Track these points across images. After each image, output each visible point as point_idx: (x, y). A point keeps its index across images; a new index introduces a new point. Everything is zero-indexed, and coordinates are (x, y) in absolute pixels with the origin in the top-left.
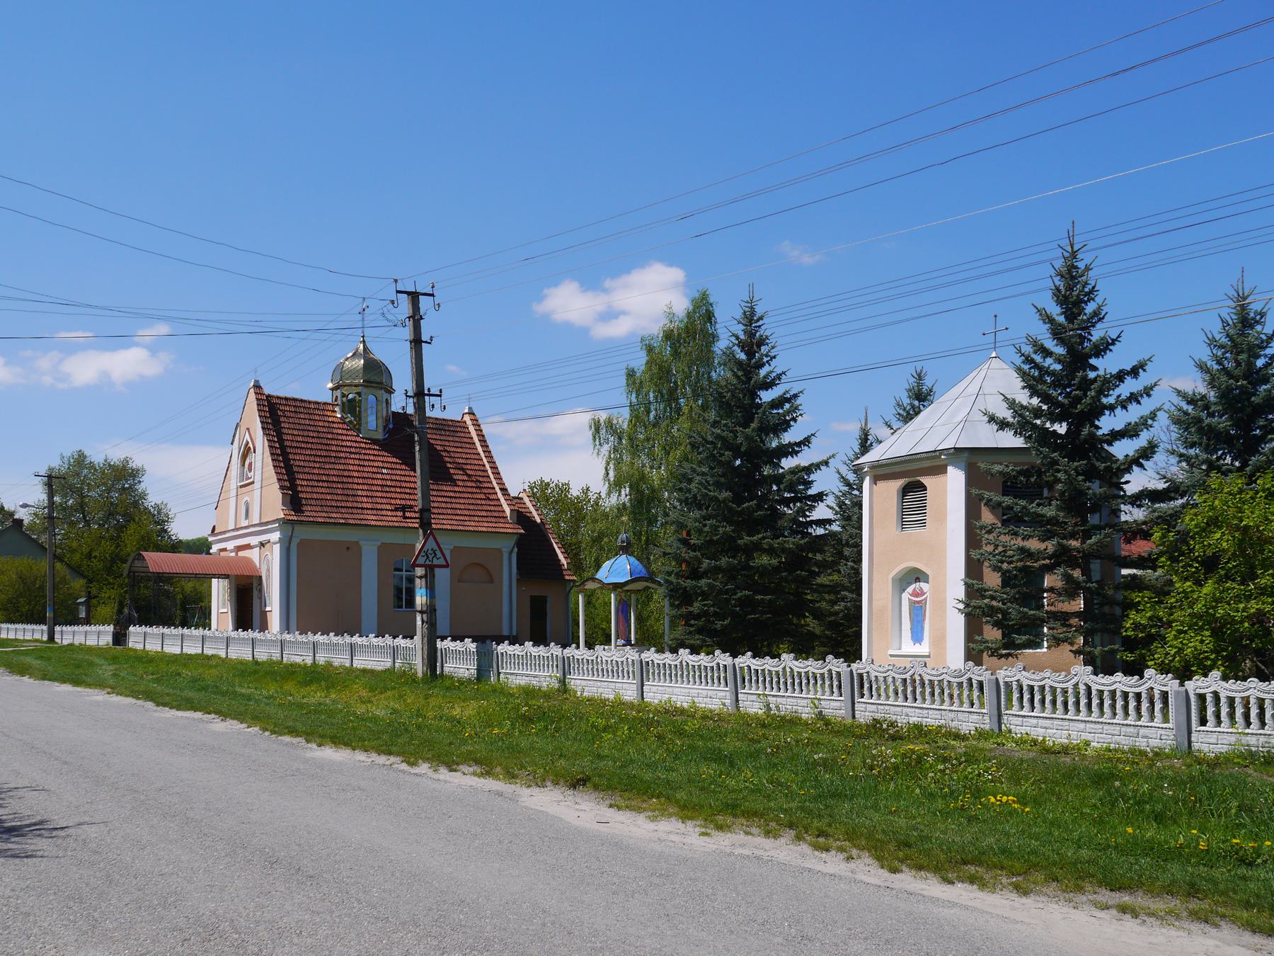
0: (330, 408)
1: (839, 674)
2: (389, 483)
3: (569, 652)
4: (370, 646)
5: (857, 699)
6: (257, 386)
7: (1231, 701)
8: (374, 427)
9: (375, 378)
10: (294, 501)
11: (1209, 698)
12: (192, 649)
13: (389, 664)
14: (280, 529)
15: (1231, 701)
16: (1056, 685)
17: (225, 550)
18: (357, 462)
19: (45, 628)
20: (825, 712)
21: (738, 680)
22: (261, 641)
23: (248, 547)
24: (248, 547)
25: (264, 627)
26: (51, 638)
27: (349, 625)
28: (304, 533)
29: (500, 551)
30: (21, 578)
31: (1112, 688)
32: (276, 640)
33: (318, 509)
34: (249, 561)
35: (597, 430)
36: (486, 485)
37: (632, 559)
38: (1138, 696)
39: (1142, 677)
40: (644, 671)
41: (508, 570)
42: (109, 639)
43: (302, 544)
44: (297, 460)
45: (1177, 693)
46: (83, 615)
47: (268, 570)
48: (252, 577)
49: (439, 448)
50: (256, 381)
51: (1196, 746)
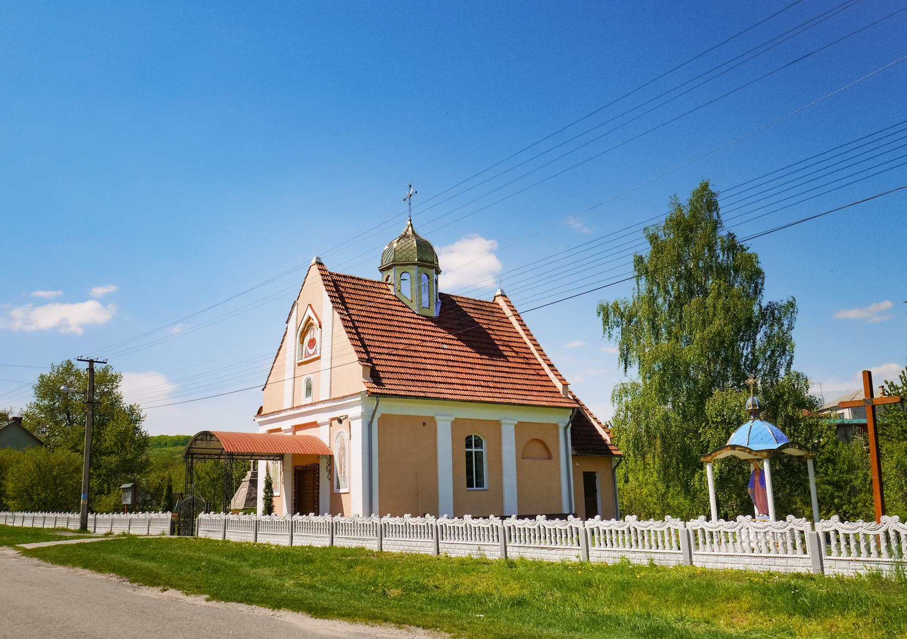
0: (384, 286)
1: (676, 530)
2: (451, 358)
3: (693, 524)
4: (239, 521)
5: (693, 552)
6: (319, 263)
7: (847, 537)
8: (426, 305)
9: (427, 257)
10: (375, 376)
11: (699, 532)
12: (321, 541)
13: (327, 543)
14: (363, 403)
15: (847, 537)
16: (776, 531)
17: (279, 430)
18: (419, 337)
19: (77, 516)
20: (656, 562)
21: (439, 533)
22: (117, 520)
23: (314, 425)
24: (314, 425)
25: (336, 508)
26: (84, 527)
27: (423, 503)
28: (388, 407)
29: (556, 426)
30: (38, 466)
31: (718, 530)
32: (354, 521)
33: (396, 382)
34: (315, 441)
35: (607, 316)
36: (532, 361)
37: (774, 428)
38: (662, 532)
39: (879, 522)
40: (383, 531)
41: (563, 447)
42: (167, 528)
43: (384, 418)
44: (367, 333)
45: (682, 531)
46: (129, 501)
47: (343, 448)
48: (318, 456)
49: (484, 326)
50: (317, 258)
51: (827, 572)
